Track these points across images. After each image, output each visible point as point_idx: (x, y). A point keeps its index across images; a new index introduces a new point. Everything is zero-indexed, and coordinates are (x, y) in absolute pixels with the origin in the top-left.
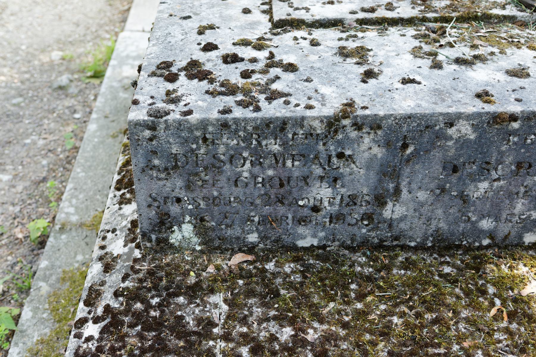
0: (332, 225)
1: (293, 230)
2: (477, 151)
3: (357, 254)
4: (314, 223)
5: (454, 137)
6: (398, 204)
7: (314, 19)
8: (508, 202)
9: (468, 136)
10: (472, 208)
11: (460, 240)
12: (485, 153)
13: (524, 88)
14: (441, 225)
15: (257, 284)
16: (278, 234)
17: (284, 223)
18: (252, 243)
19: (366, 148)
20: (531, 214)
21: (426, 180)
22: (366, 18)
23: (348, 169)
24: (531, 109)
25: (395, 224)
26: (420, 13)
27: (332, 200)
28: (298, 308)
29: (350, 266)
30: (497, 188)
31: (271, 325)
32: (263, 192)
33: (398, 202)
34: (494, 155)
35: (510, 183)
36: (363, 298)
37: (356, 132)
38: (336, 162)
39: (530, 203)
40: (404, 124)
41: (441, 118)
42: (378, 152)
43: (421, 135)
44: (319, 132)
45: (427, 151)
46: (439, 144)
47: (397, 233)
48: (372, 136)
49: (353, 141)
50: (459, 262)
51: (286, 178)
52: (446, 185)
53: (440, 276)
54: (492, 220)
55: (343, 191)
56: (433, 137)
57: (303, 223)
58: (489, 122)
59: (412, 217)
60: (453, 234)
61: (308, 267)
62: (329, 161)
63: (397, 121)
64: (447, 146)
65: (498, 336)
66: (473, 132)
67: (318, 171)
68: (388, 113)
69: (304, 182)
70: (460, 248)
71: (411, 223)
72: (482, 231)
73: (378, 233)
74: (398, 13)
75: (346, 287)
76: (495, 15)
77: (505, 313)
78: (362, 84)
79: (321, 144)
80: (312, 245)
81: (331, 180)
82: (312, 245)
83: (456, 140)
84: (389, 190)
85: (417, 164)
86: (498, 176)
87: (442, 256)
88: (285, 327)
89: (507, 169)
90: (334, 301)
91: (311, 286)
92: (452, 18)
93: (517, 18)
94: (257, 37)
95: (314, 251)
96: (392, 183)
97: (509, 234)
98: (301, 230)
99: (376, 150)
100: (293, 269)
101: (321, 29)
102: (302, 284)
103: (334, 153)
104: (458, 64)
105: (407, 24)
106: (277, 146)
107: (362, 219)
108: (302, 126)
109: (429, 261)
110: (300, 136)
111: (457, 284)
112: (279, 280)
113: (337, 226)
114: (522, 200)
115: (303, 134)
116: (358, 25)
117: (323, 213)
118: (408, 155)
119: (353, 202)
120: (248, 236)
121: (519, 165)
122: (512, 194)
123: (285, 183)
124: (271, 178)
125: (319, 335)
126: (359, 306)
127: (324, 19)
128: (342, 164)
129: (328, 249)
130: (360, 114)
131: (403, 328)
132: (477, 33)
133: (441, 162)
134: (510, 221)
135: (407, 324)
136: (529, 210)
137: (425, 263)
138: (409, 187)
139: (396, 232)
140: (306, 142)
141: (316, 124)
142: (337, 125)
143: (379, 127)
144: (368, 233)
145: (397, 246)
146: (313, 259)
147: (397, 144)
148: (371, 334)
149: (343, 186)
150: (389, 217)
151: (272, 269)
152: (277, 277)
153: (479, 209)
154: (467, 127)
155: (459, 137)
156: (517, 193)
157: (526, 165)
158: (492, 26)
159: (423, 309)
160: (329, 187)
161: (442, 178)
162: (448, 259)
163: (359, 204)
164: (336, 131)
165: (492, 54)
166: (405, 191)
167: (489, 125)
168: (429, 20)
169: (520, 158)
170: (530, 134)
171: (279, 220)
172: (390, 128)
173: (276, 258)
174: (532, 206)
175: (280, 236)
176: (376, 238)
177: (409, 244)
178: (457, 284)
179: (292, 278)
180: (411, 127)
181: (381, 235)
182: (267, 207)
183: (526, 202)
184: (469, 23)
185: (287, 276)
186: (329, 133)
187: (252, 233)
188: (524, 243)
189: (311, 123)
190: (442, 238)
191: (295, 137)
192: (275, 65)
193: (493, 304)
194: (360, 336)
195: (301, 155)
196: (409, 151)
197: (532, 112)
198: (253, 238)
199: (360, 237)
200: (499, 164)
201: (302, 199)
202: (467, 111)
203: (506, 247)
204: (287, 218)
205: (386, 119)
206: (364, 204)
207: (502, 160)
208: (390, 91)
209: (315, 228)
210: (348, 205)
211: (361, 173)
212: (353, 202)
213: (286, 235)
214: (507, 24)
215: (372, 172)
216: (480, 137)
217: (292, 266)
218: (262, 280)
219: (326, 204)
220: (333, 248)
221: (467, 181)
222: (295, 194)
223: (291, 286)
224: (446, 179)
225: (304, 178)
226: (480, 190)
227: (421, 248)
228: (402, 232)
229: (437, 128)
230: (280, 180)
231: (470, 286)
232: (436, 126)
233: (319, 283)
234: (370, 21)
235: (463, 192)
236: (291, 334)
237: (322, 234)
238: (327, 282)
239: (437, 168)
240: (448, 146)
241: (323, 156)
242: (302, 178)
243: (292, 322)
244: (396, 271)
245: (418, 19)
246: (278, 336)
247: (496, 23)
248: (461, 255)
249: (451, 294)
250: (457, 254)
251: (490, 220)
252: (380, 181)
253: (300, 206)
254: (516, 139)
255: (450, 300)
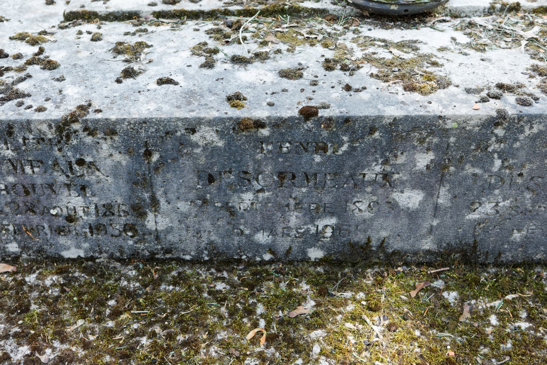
0: (94, 235)
1: (54, 240)
2: (230, 159)
3: (130, 267)
4: (74, 233)
5: (200, 143)
6: (159, 215)
7: (107, 11)
8: (280, 215)
9: (215, 144)
10: (242, 221)
11: (238, 254)
12: (239, 162)
13: (287, 91)
14: (213, 238)
15: (10, 297)
16: (39, 244)
17: (42, 233)
18: (14, 253)
19: (107, 155)
20: (308, 228)
21: (183, 190)
22: (163, 11)
23: (94, 177)
24: (278, 115)
25: (162, 236)
26: (224, 5)
27: (86, 209)
28: (43, 325)
29: (116, 281)
30: (264, 199)
31: (9, 343)
32: (9, 200)
33: (159, 213)
34: (250, 164)
35: (276, 195)
36: (116, 316)
37: (91, 137)
38: (78, 170)
39: (305, 215)
40: (141, 129)
41: (180, 124)
42: (122, 159)
43: (163, 142)
44: (50, 136)
45: (175, 159)
46: (185, 151)
47: (168, 245)
48: (109, 141)
49: (90, 148)
50: (236, 278)
51: (30, 186)
52: (206, 196)
53: (210, 293)
54: (268, 234)
55: (95, 199)
56: (177, 143)
57: (62, 233)
58: (234, 129)
59: (179, 229)
60: (228, 248)
61: (70, 280)
62: (71, 168)
63: (132, 126)
64: (195, 154)
65: (249, 362)
66: (220, 140)
67: (62, 179)
68: (120, 117)
69: (49, 189)
70: (241, 262)
71: (180, 235)
72: (259, 245)
73: (146, 245)
74: (201, 5)
75: (103, 303)
76: (303, 8)
77: (264, 336)
78: (116, 84)
79: (56, 149)
80: (79, 256)
81: (79, 188)
82: (79, 256)
83: (204, 147)
84: (146, 200)
85: (168, 172)
86: (261, 187)
87: (219, 271)
88: (23, 346)
89: (268, 179)
90: (84, 317)
91: (66, 301)
92: (256, 11)
93: (328, 11)
94: (39, 31)
95: (82, 262)
96: (147, 193)
97: (290, 248)
98: (62, 240)
99: (117, 157)
100: (54, 281)
101: (116, 22)
102: (57, 299)
103: (73, 160)
104: (233, 63)
105: (208, 17)
106: (9, 151)
107: (125, 231)
108: (30, 131)
109: (204, 276)
110: (31, 141)
111: (223, 303)
112: (35, 294)
113: (100, 236)
114: (296, 213)
115: (33, 139)
116: (155, 19)
117: (81, 222)
118: (155, 163)
119: (110, 212)
120: (7, 245)
121: (281, 175)
122: (283, 206)
123: (30, 190)
124: (14, 186)
125: (56, 355)
126: (111, 324)
127: (118, 12)
128: (85, 172)
129: (98, 261)
130: (90, 118)
131: (148, 350)
132: (278, 28)
133: (194, 171)
134: (288, 235)
135: (154, 347)
136: (305, 224)
137: (198, 279)
138: (166, 197)
139: (165, 244)
140: (40, 147)
141: (44, 128)
142: (68, 129)
143: (113, 132)
144: (135, 245)
145: (172, 259)
146: (79, 272)
147: (140, 151)
148: (111, 356)
149: (93, 195)
150: (154, 229)
151: (32, 281)
152: (34, 290)
153: (250, 221)
154: (211, 133)
155: (206, 145)
156: (288, 205)
157: (290, 176)
158: (296, 20)
159: (178, 330)
160: (79, 196)
161: (199, 188)
162: (225, 274)
163: (116, 213)
164: (68, 137)
165: (279, 51)
166: (162, 201)
167: (236, 132)
168: (232, 14)
169: (280, 168)
170: (284, 142)
171: (36, 230)
172: (126, 133)
173: (41, 270)
174: (307, 219)
175: (41, 246)
176: (146, 251)
177: (184, 257)
178: (223, 303)
179: (50, 292)
180: (150, 133)
181: (151, 247)
182: (19, 216)
183: (300, 215)
184: (275, 17)
185: (45, 290)
186: (62, 138)
187: (11, 242)
188: (310, 258)
189: (39, 127)
190: (218, 252)
191: (27, 141)
192: (35, 62)
193: (255, 325)
194: (100, 357)
195: (38, 161)
196: (155, 157)
197: (279, 118)
198: (13, 248)
199: (128, 249)
200: (259, 174)
201: (54, 208)
202: (208, 116)
203: (291, 262)
204: (44, 228)
205: (119, 123)
206: (122, 214)
207: (260, 170)
208: (139, 92)
209: (76, 238)
210: (105, 215)
211: (109, 181)
212: (110, 212)
213: (47, 245)
214: (317, 18)
215: (121, 180)
216: (228, 144)
217: (54, 279)
218: (16, 294)
219: (81, 213)
220: (102, 259)
221: (228, 192)
222: (45, 203)
223: (44, 300)
224: (204, 189)
225: (49, 185)
226: (245, 201)
227: (196, 262)
228: (172, 244)
229: (179, 134)
230: (24, 187)
231: (238, 305)
232: (176, 132)
233: (75, 299)
234: (169, 14)
235: (227, 203)
236: (26, 353)
237: (86, 245)
238: (85, 297)
239: (191, 178)
240: (197, 154)
241: (62, 162)
242: (47, 186)
243: (32, 340)
244: (165, 286)
245: (220, 12)
246: (12, 355)
247: (305, 17)
248: (241, 270)
249: (213, 313)
250: (237, 269)
251: (265, 234)
252: (133, 190)
253: (53, 215)
254: (270, 147)
255: (211, 320)
